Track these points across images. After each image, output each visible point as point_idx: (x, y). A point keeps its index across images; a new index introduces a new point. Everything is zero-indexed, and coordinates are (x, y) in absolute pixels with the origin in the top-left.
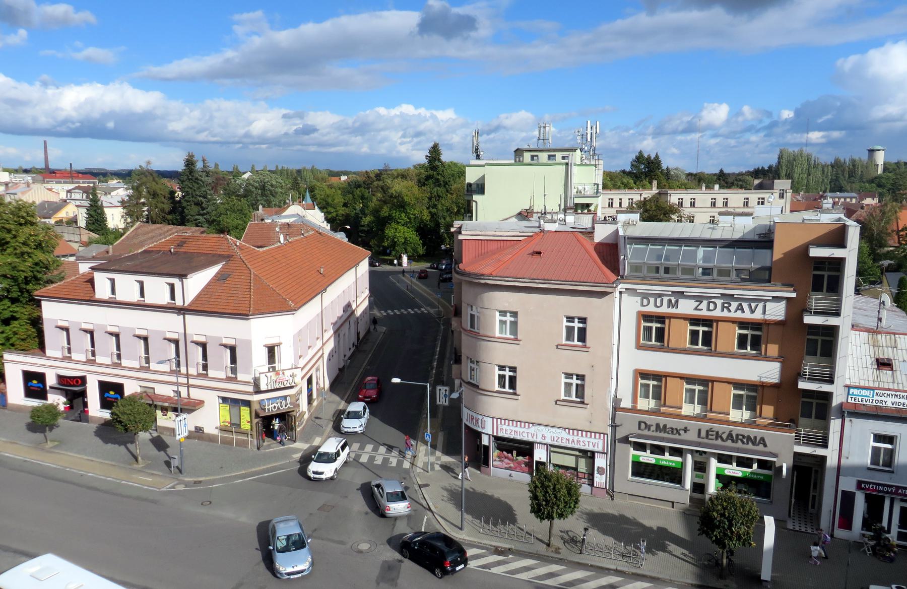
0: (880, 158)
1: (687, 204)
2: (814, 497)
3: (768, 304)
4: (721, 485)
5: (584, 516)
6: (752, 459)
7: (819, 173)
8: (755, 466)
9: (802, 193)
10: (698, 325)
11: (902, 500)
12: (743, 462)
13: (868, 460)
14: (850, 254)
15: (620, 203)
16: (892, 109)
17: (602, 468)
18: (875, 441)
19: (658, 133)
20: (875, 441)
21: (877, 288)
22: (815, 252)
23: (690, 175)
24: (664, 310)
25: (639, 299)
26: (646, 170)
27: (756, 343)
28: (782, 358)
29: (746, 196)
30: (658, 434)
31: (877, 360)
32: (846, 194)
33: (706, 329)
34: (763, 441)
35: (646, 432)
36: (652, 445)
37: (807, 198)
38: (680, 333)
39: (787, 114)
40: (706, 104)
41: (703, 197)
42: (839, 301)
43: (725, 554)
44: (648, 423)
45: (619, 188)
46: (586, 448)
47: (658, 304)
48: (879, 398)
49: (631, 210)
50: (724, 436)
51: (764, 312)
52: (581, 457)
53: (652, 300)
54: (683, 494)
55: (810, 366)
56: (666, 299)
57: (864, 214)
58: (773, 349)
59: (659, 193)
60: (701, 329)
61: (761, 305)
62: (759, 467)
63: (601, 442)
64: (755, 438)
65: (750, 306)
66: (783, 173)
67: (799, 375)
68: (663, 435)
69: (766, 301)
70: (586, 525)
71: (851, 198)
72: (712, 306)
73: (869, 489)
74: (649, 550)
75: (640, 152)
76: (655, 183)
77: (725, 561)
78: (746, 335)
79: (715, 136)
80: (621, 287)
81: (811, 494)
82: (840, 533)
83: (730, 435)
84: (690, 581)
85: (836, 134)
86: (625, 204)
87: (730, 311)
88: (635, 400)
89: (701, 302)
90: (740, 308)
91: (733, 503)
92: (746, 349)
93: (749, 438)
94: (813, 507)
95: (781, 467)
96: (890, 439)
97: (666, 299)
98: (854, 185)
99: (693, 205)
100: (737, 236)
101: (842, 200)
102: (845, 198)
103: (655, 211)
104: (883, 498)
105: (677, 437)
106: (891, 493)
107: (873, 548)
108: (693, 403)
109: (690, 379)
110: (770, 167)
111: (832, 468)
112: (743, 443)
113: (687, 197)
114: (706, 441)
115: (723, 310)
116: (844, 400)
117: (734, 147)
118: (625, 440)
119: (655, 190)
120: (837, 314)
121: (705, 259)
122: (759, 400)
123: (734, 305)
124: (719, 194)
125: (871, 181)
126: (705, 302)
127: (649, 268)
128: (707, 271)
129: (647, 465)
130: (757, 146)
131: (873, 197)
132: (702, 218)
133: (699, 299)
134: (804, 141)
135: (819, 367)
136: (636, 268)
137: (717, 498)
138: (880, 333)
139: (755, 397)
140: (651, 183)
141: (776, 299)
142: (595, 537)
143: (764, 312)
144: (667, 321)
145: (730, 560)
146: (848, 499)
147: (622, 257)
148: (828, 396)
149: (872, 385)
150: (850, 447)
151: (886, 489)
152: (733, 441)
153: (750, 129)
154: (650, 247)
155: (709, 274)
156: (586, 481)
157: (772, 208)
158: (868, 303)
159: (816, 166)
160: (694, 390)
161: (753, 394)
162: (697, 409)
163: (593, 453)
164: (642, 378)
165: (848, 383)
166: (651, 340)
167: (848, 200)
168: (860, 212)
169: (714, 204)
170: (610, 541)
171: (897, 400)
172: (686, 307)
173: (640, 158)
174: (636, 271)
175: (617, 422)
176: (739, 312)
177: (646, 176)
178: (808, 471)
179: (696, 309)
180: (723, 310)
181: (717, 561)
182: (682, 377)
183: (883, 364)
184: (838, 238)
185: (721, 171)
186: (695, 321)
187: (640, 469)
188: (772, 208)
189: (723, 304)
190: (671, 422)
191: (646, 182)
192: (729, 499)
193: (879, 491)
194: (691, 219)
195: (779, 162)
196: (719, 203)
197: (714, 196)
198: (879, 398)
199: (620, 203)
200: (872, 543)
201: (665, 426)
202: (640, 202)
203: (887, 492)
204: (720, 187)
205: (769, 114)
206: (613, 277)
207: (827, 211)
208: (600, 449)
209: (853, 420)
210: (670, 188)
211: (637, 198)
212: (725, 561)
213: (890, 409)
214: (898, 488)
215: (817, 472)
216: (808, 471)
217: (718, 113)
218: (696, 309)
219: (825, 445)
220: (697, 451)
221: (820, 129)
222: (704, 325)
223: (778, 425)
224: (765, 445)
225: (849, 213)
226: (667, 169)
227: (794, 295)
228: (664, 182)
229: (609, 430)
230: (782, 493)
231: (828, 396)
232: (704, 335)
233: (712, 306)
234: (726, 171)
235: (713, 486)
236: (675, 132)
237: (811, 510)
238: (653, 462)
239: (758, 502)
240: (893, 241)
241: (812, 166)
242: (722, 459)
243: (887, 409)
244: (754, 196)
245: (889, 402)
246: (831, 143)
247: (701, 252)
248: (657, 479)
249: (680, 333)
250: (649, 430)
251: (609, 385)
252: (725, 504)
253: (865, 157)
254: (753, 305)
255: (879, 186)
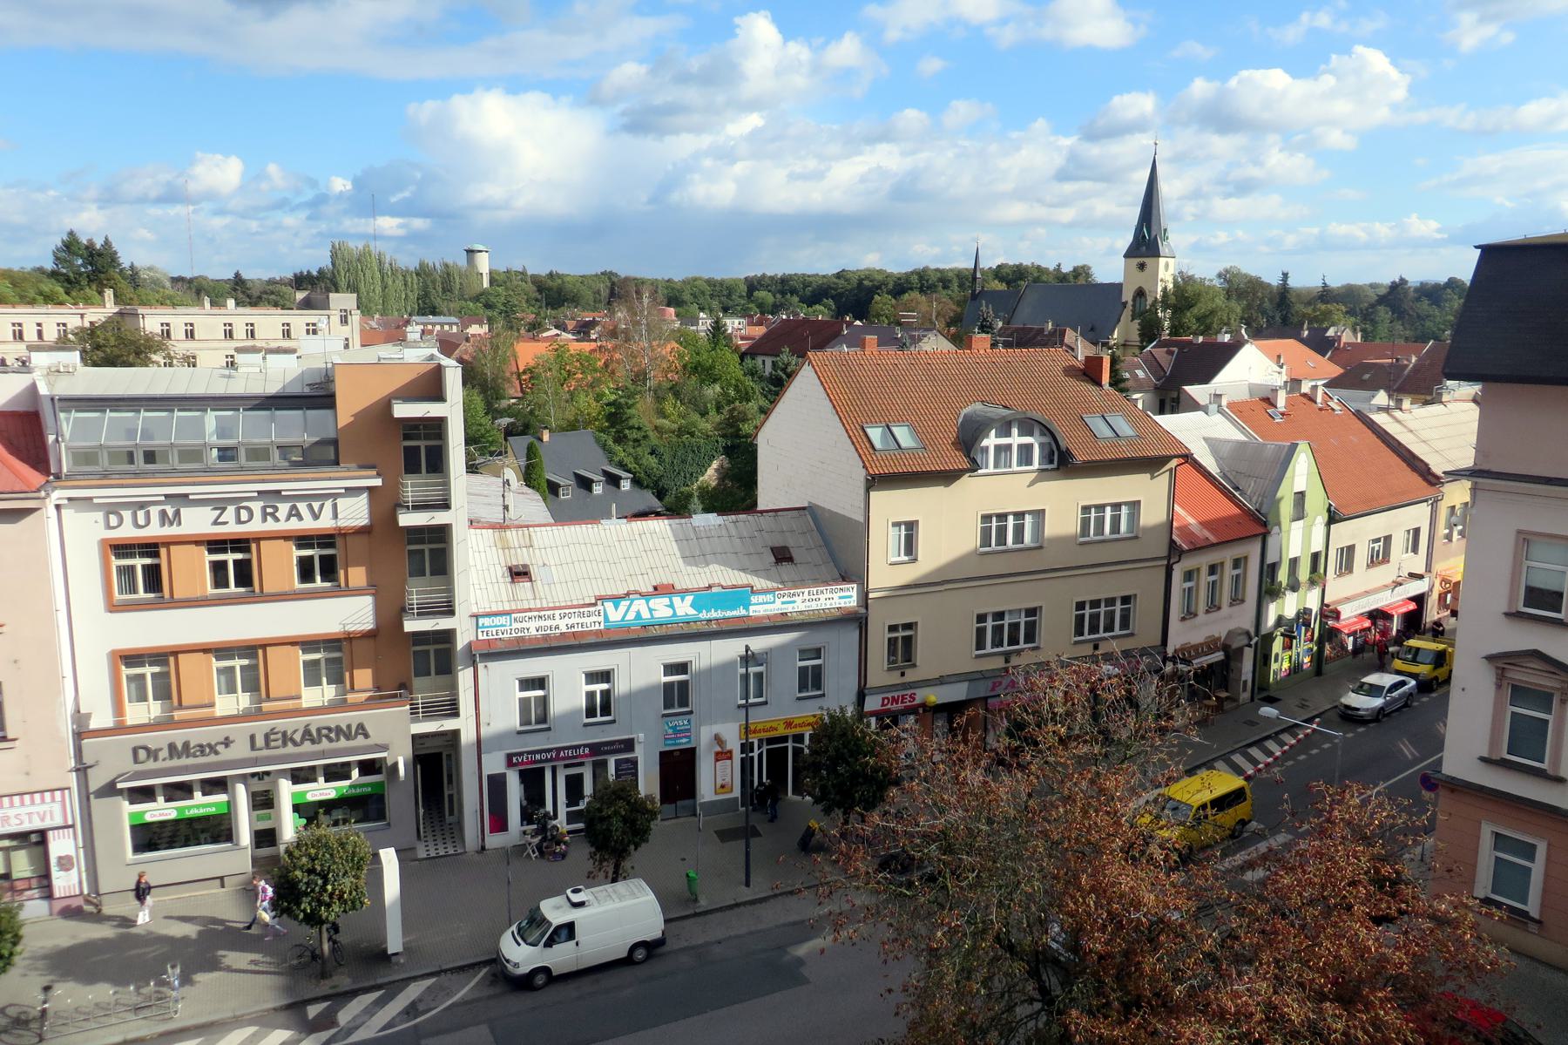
0: (484, 264)
1: (178, 333)
2: (451, 796)
3: (339, 501)
4: (304, 821)
5: (40, 964)
6: (348, 764)
7: (399, 283)
8: (355, 773)
9: (377, 316)
10: (224, 551)
11: (566, 766)
12: (333, 773)
13: (514, 721)
14: (452, 409)
15: (40, 334)
16: (492, 191)
17: (69, 858)
18: (521, 690)
19: (110, 198)
20: (521, 690)
21: (498, 461)
22: (402, 410)
23: (176, 280)
24: (155, 530)
25: (100, 516)
26: (86, 268)
27: (329, 569)
28: (373, 588)
29: (286, 319)
30: (176, 762)
31: (510, 569)
32: (442, 319)
33: (239, 556)
34: (362, 730)
35: (151, 765)
36: (166, 786)
37: (386, 325)
38: (190, 570)
39: (340, 185)
40: (199, 154)
41: (208, 321)
42: (446, 485)
43: (325, 936)
44: (152, 746)
45: (32, 302)
46: (26, 827)
47: (141, 521)
48: (519, 625)
49: (62, 344)
50: (297, 737)
51: (335, 516)
52: (15, 848)
53: (127, 515)
54: (237, 858)
55: (418, 593)
56: (154, 511)
57: (471, 350)
58: (357, 575)
59: (120, 314)
60: (230, 557)
61: (328, 504)
62: (362, 773)
63: (57, 808)
64: (349, 727)
65: (310, 507)
66: (343, 283)
67: (403, 611)
68: (184, 761)
69: (335, 496)
70: (45, 981)
71: (451, 324)
72: (244, 515)
73: (522, 763)
74: (186, 980)
75: (71, 233)
76: (109, 293)
77: (326, 947)
78: (311, 558)
79: (220, 212)
80: (58, 495)
81: (446, 793)
82: (494, 841)
83: (307, 733)
84: (271, 1005)
85: (419, 223)
86: (51, 334)
87: (277, 520)
88: (119, 709)
89: (224, 509)
90: (294, 513)
91: (326, 845)
92: (313, 581)
93: (339, 730)
94: (451, 813)
95: (396, 764)
96: (540, 683)
97: (154, 511)
98: (452, 305)
99: (190, 335)
100: (273, 389)
101: (438, 328)
102: (442, 325)
103: (111, 347)
104: (542, 770)
105: (212, 758)
106: (551, 760)
107: (539, 847)
108: (234, 691)
109: (222, 651)
110: (321, 271)
111: (469, 746)
112: (331, 740)
113: (178, 320)
114: (266, 752)
115: (264, 520)
116: (473, 638)
117: (257, 233)
118: (110, 790)
119: (110, 308)
120: (446, 506)
121: (222, 432)
122: (345, 663)
123: (283, 508)
124: (236, 315)
125: (476, 299)
126: (231, 510)
127: (114, 455)
128: (229, 453)
129: (163, 824)
130: (296, 235)
131: (481, 324)
132: (211, 358)
133: (220, 504)
134: (371, 231)
135: (431, 592)
136: (85, 457)
137: (298, 846)
138: (508, 527)
139: (338, 661)
140: (101, 293)
141: (351, 492)
142: (69, 995)
143: (335, 516)
144: (163, 551)
145: (335, 942)
146: (497, 785)
147: (51, 438)
148: (448, 636)
149: (507, 608)
150: (488, 707)
151: (544, 756)
152: (313, 742)
153: (281, 205)
154: (109, 414)
155: (232, 459)
156: (35, 893)
157: (329, 341)
158: (486, 484)
159: (394, 272)
160: (143, 676)
161: (335, 655)
162: (242, 701)
163: (42, 834)
164: (128, 665)
165: (475, 610)
166: (135, 591)
167: (446, 328)
168: (464, 346)
169: (229, 334)
170: (104, 992)
171: (542, 623)
172: (197, 521)
173: (71, 245)
174: (88, 463)
175: (87, 760)
176: (294, 519)
177: (90, 281)
178: (436, 762)
179: (216, 523)
180: (264, 520)
181: (313, 952)
182: (206, 650)
183: (519, 574)
184: (431, 387)
185: (237, 275)
186: (216, 545)
187: (149, 838)
188: (329, 341)
189: (264, 508)
190: (196, 735)
191: (91, 292)
192: (318, 842)
193: (535, 762)
194: (190, 361)
195: (333, 264)
196: (240, 332)
197: (228, 320)
198: (519, 625)
199: (40, 334)
200: (537, 840)
201: (186, 745)
202: (83, 329)
203: (547, 760)
204: (237, 304)
205: (313, 183)
206: (36, 478)
207: (414, 345)
208: (59, 821)
209: (490, 664)
210: (143, 304)
211: (74, 322)
212: (326, 947)
213: (537, 639)
214: (558, 750)
215: (449, 756)
216: (436, 762)
217: (222, 173)
218: (216, 523)
219: (455, 713)
220: (253, 775)
221: (393, 213)
222: (234, 550)
223: (381, 697)
224: (366, 736)
225: (447, 346)
226: (132, 267)
227: (378, 482)
228: (128, 292)
229: (73, 780)
230: (402, 804)
231: (448, 636)
232: (236, 565)
233: (244, 515)
234: (245, 275)
235: (289, 827)
236: (143, 200)
237: (449, 819)
238: (173, 815)
239: (367, 831)
240: (513, 390)
241: (388, 273)
242: (299, 776)
243: (531, 640)
244: (299, 320)
245: (532, 628)
246: (414, 237)
247: (211, 419)
248: (186, 845)
249: (190, 570)
250: (156, 759)
251: (60, 692)
252: (313, 851)
253: (462, 261)
254: (316, 505)
255: (488, 306)
